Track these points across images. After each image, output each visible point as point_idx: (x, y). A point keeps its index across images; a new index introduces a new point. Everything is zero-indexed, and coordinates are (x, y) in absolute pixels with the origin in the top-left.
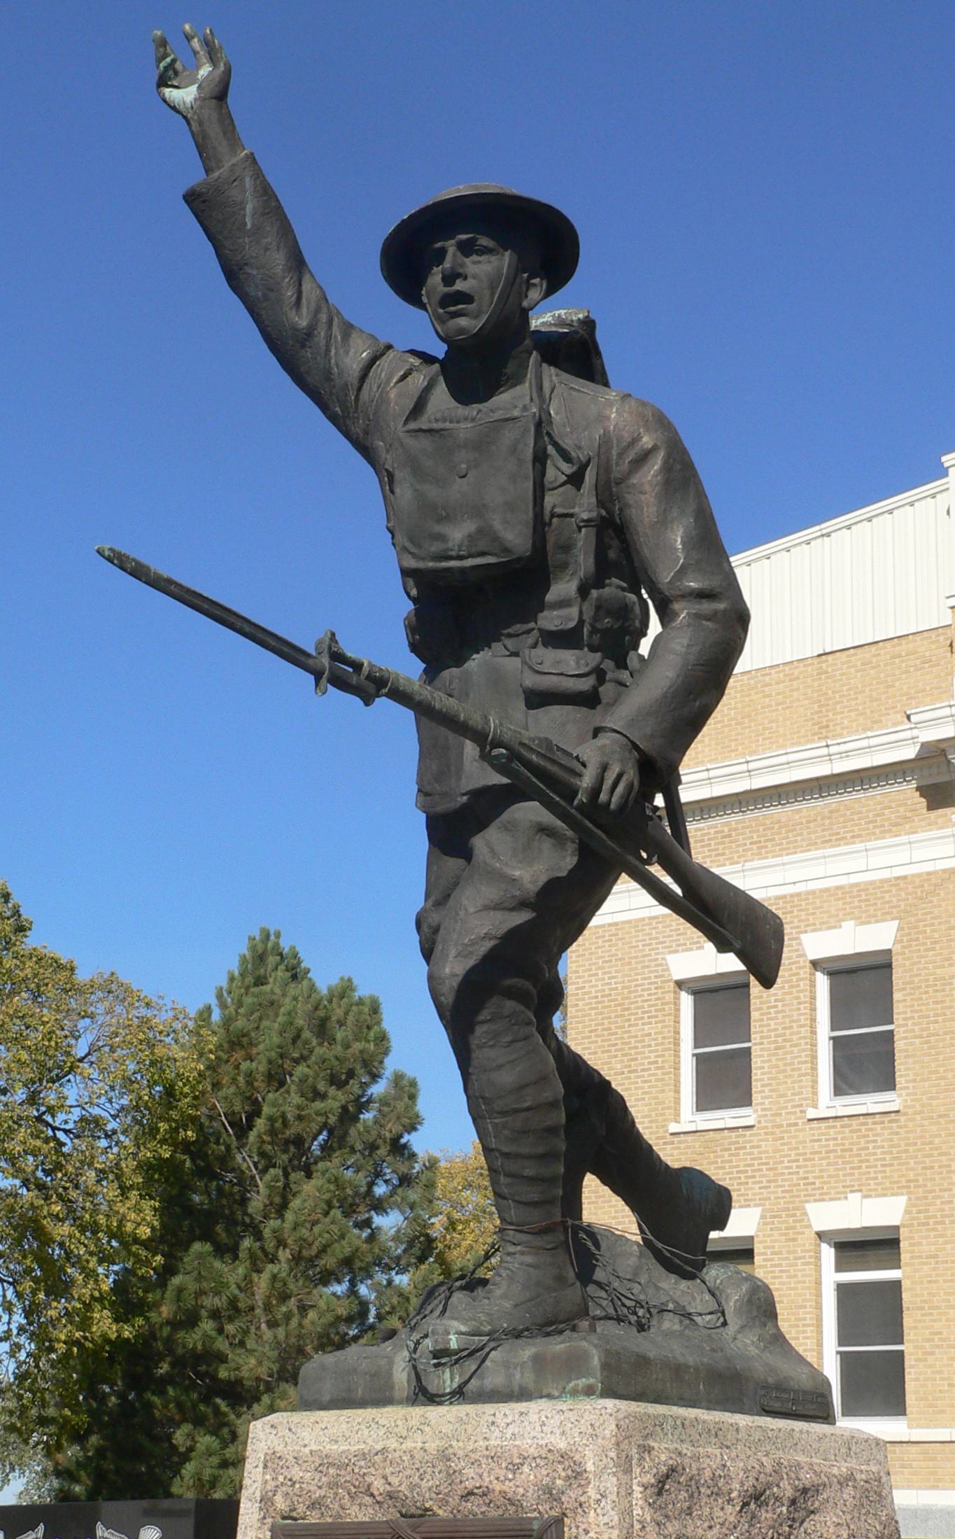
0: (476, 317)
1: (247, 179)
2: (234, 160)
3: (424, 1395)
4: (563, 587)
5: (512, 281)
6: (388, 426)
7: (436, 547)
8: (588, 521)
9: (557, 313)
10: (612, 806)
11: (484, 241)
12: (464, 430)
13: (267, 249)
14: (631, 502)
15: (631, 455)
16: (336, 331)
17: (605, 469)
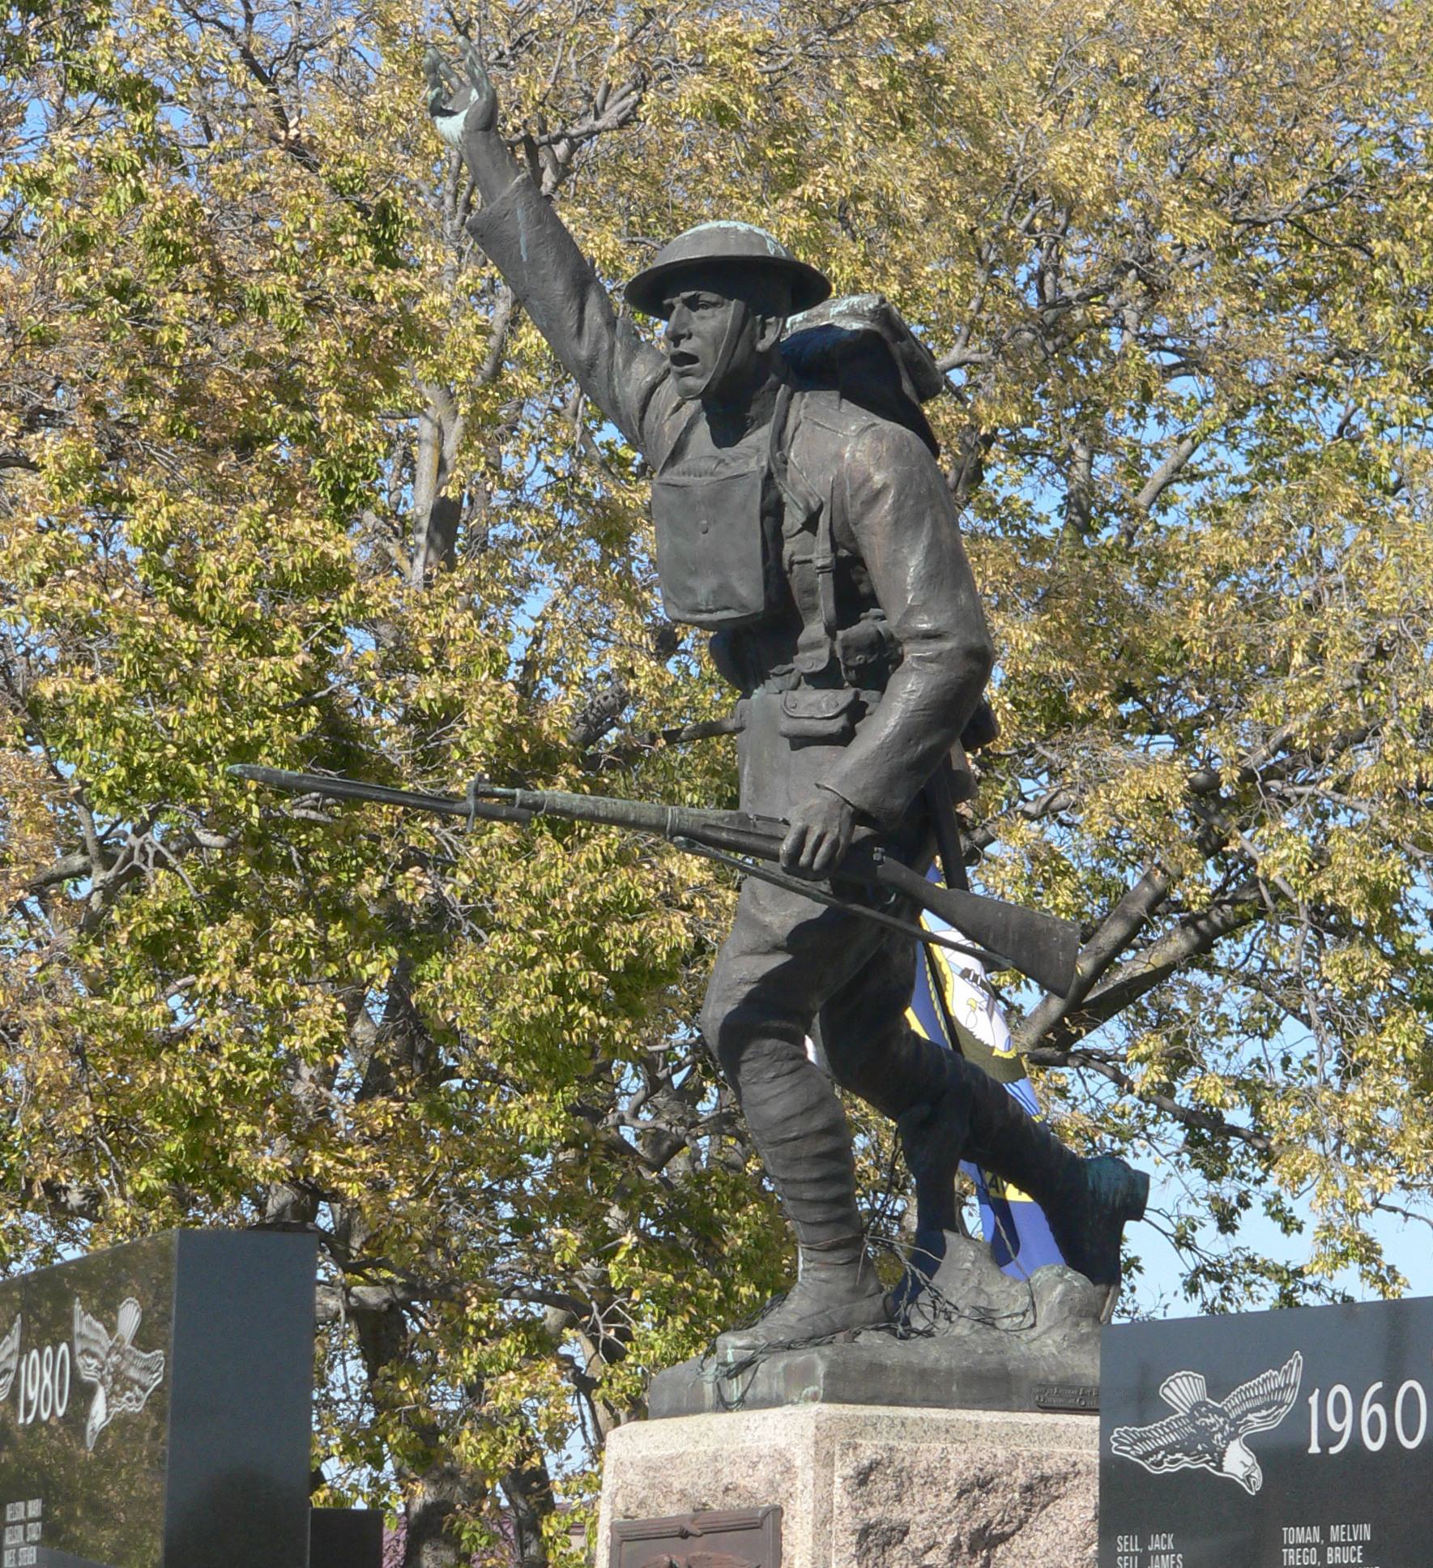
0: (701, 376)
2: (506, 192)
3: (723, 1405)
4: (814, 629)
7: (689, 601)
10: (816, 866)
11: (707, 296)
15: (864, 494)
17: (840, 511)
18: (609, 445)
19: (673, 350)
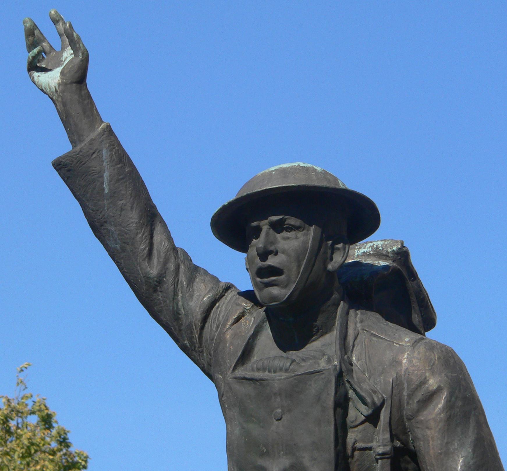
0: (286, 286)
1: (104, 152)
2: (93, 135)
8: (383, 454)
9: (376, 243)
11: (292, 221)
12: (278, 380)
13: (122, 210)
14: (420, 436)
15: (419, 395)
16: (183, 279)
17: (398, 407)
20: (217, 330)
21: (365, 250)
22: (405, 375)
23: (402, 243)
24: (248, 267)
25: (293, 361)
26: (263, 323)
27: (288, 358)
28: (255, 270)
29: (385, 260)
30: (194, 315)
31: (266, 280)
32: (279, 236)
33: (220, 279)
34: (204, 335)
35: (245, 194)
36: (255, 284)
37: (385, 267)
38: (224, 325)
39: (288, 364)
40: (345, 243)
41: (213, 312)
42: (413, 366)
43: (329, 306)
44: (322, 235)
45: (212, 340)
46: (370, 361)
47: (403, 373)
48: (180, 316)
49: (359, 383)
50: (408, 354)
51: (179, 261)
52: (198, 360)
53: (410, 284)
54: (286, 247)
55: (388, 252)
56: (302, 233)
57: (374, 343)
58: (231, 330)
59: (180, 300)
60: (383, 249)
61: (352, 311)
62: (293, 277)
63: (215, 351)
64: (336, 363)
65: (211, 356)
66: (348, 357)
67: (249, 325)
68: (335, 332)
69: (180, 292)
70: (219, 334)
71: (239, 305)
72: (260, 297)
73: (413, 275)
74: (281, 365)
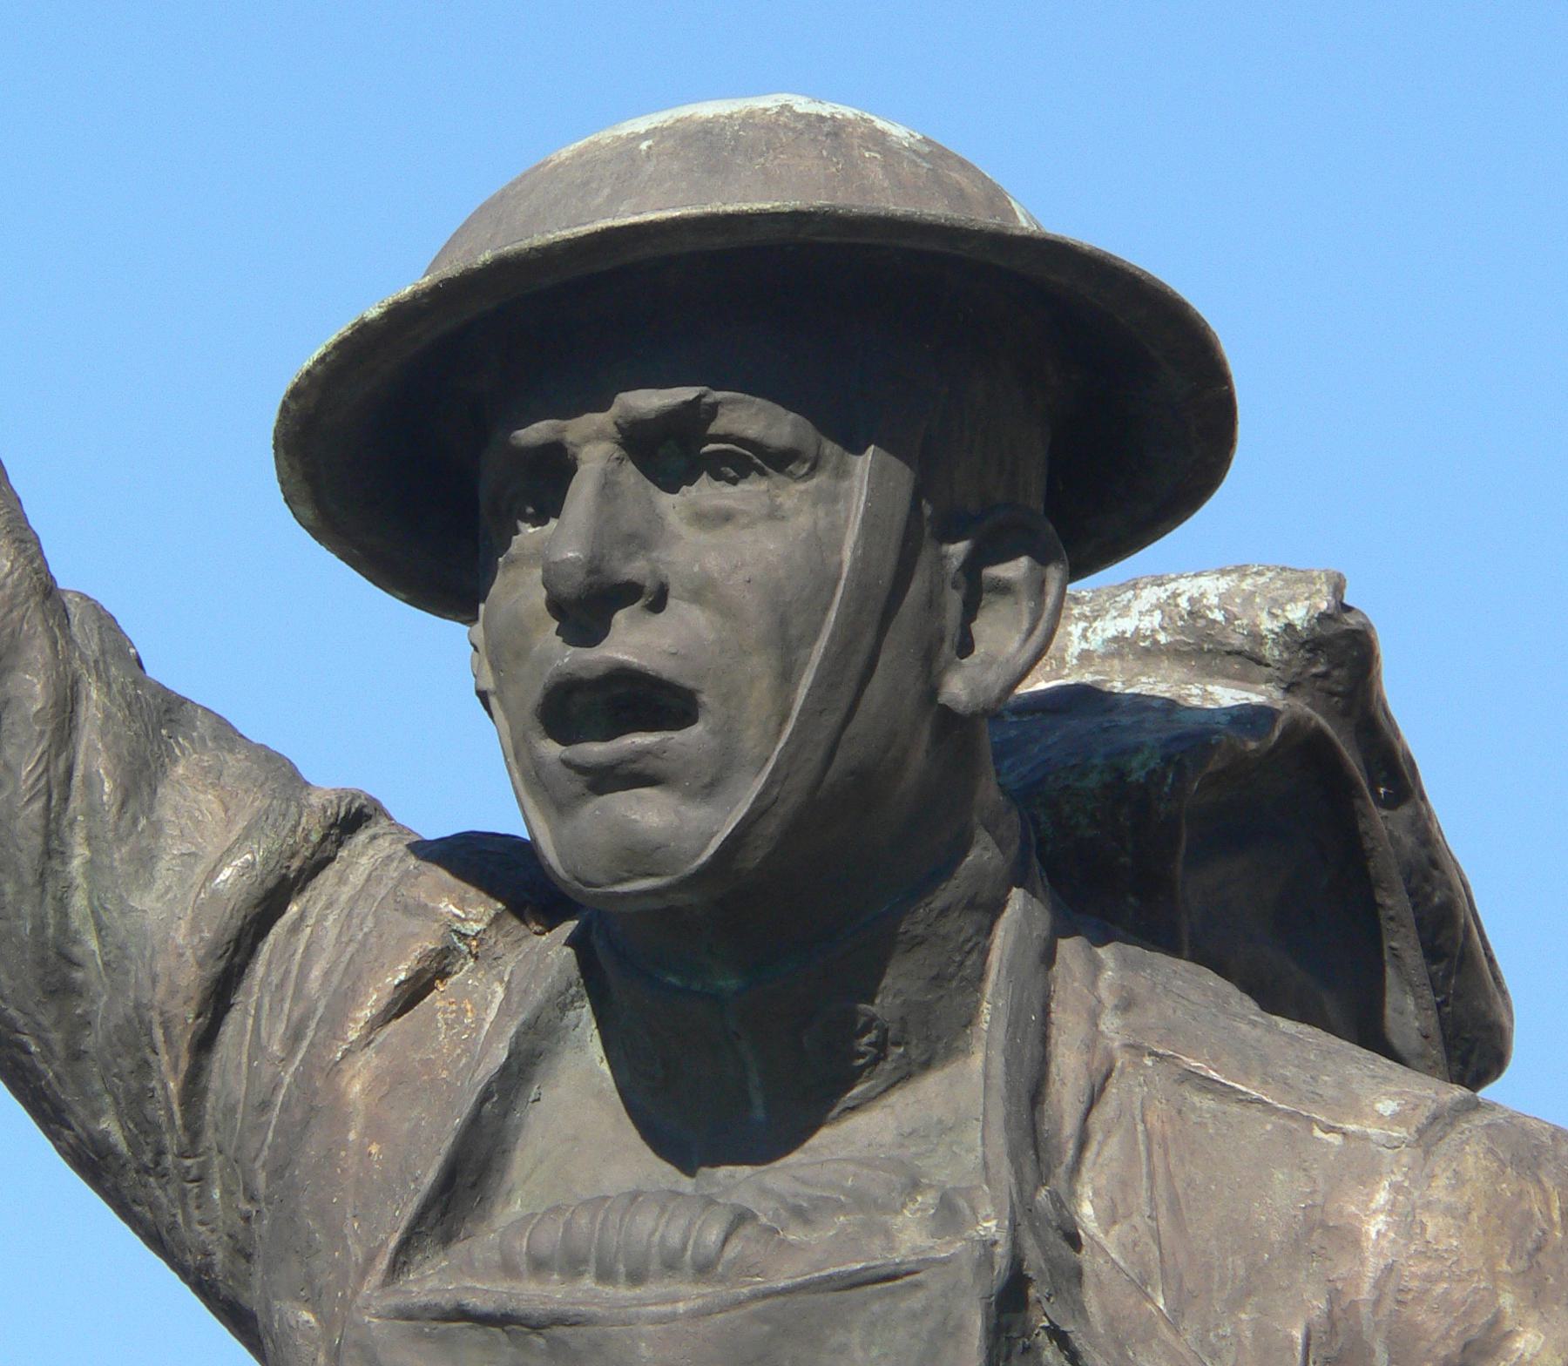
0: (710, 788)
5: (882, 600)
6: (336, 1235)
11: (748, 417)
16: (97, 761)
18: (1509, 1262)
19: (570, 658)
20: (291, 1050)
21: (1128, 625)
22: (1377, 1303)
23: (1338, 588)
24: (489, 683)
25: (742, 1217)
26: (564, 1008)
27: (710, 1201)
28: (534, 694)
29: (1243, 679)
30: (159, 967)
31: (595, 751)
32: (672, 505)
33: (307, 775)
34: (215, 1083)
35: (486, 256)
36: (533, 780)
37: (1249, 718)
38: (335, 1019)
39: (713, 1235)
40: (1042, 558)
41: (266, 948)
42: (1422, 1255)
43: (944, 912)
44: (915, 507)
45: (265, 1106)
46: (1179, 1225)
47: (1366, 1292)
48: (78, 975)
49: (1120, 1345)
50: (1396, 1188)
51: (76, 664)
52: (173, 1227)
53: (1382, 823)
54: (713, 563)
55: (1256, 637)
56: (801, 486)
57: (1202, 1125)
58: (370, 1052)
59: (80, 880)
60: (1230, 618)
61: (1069, 948)
62: (750, 739)
63: (277, 1172)
64: (990, 1226)
65: (252, 1199)
66: (1055, 1198)
67: (479, 1021)
68: (977, 1061)
69: (79, 836)
70: (304, 1078)
71: (422, 911)
72: (560, 855)
73: (1395, 775)
74: (675, 1239)
